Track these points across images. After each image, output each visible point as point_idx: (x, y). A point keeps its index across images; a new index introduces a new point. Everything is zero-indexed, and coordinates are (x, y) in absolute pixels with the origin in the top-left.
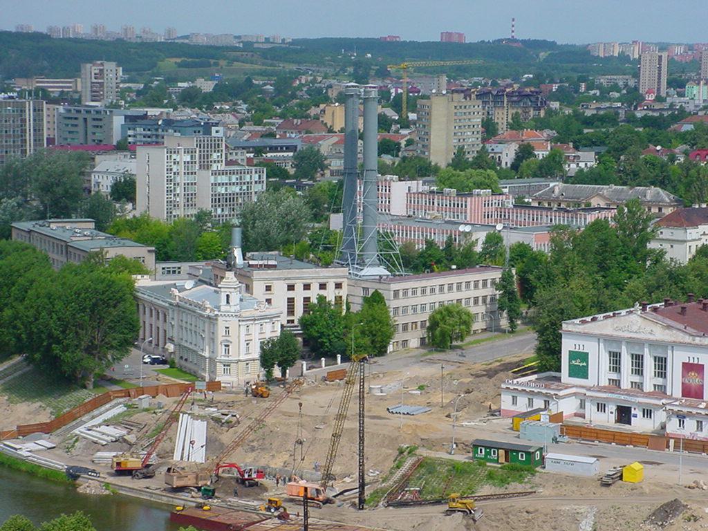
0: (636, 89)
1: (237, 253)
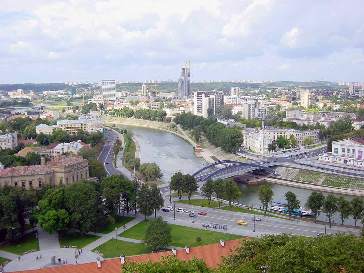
0: (348, 92)
1: (263, 126)
